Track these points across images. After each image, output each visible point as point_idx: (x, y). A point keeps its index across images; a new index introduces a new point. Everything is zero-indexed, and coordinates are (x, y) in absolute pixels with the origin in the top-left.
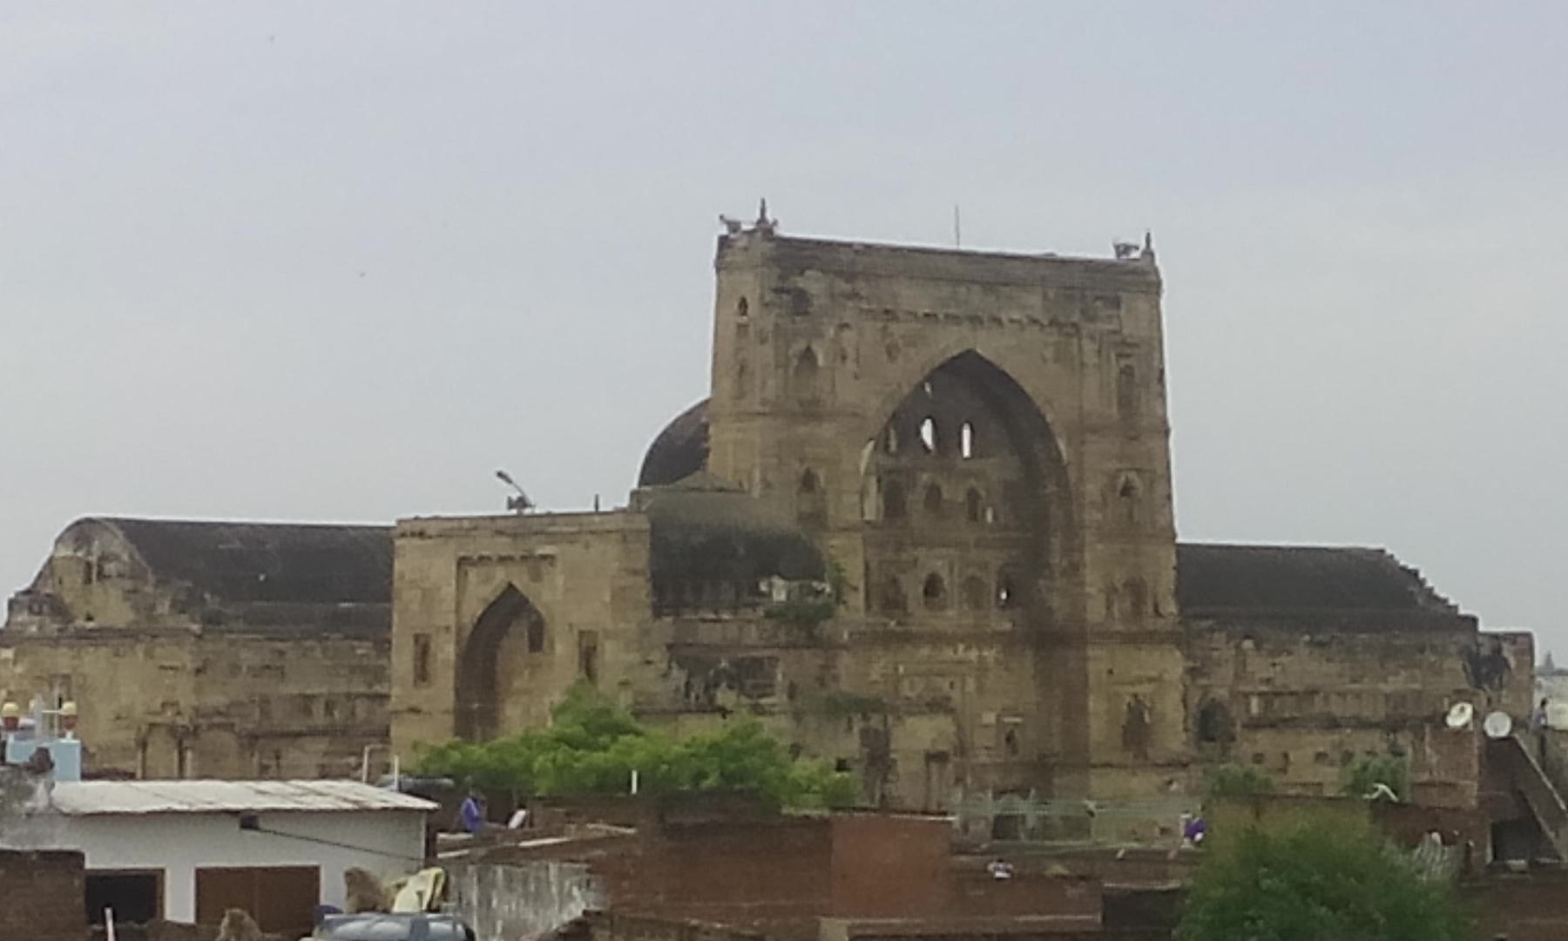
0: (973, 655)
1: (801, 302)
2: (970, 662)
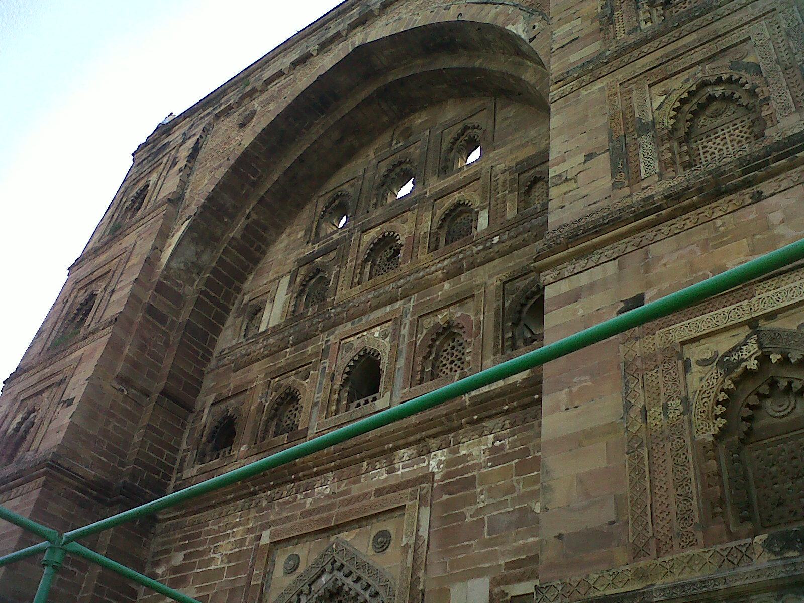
0: (436, 462)
2: (428, 477)
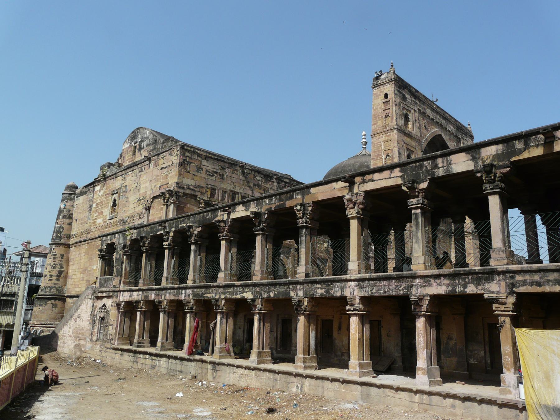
1: (404, 98)
